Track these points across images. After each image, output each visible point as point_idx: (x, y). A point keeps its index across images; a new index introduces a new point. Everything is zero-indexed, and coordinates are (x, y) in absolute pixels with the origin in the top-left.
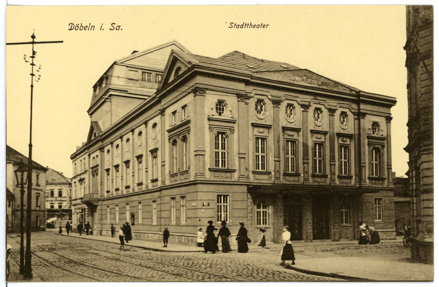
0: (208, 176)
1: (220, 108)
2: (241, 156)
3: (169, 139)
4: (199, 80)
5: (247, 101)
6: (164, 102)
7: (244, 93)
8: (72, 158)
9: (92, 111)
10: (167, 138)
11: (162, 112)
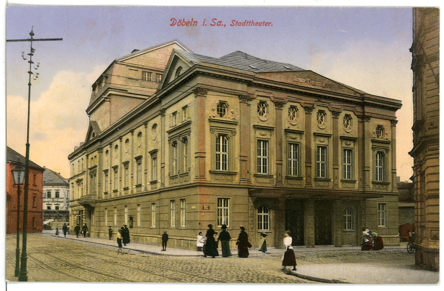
0: (209, 178)
1: (221, 109)
2: (242, 158)
3: (169, 141)
4: (200, 81)
5: (249, 102)
6: (164, 102)
7: (245, 94)
8: (69, 159)
9: (90, 111)
10: (167, 139)
11: (162, 113)
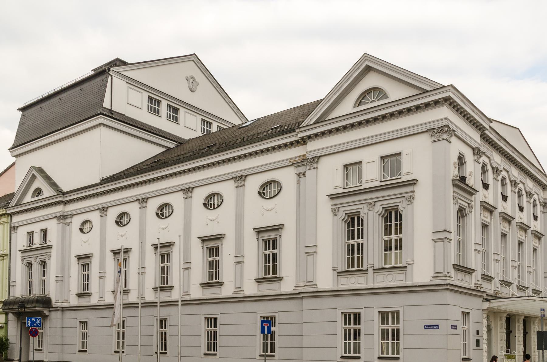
4: (443, 113)
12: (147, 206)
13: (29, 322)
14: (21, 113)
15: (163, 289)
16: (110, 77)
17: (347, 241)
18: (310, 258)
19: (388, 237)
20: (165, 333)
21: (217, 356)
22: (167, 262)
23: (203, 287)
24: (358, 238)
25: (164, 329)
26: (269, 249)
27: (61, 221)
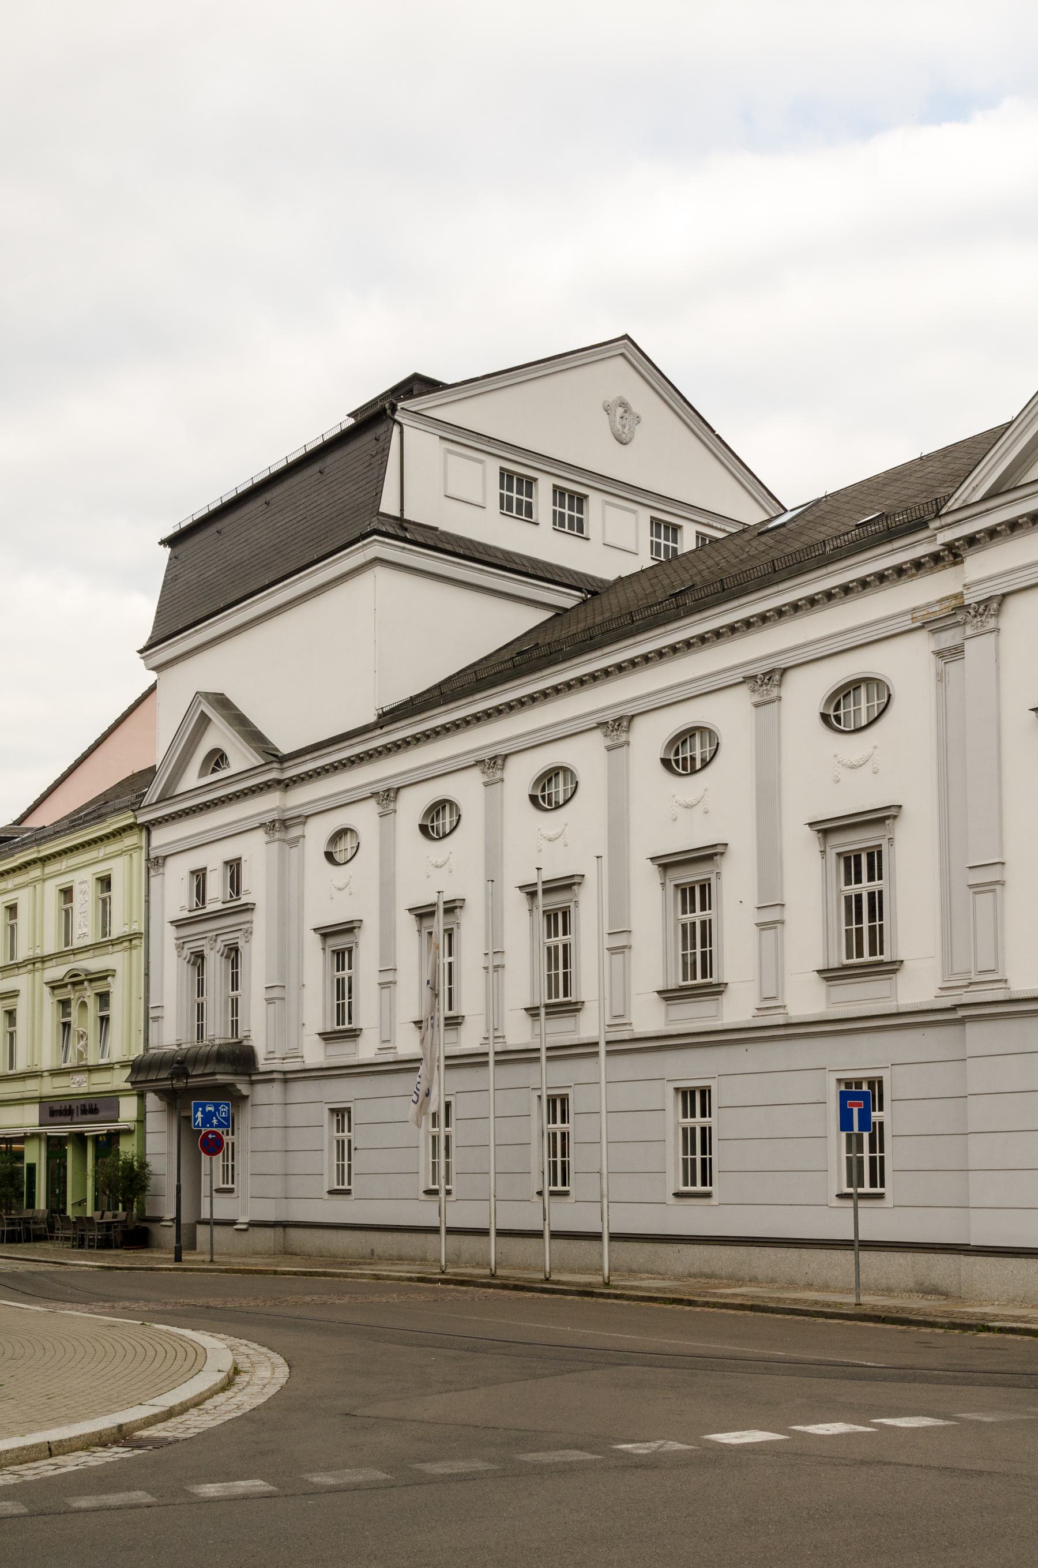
12: (783, 694)
13: (199, 1115)
14: (168, 550)
15: (555, 1010)
16: (396, 430)
17: (681, 916)
18: (984, 900)
19: (854, 889)
20: (563, 1135)
21: (888, 1201)
22: (703, 909)
23: (666, 999)
24: (871, 878)
25: (559, 1124)
26: (858, 880)
27: (277, 835)
